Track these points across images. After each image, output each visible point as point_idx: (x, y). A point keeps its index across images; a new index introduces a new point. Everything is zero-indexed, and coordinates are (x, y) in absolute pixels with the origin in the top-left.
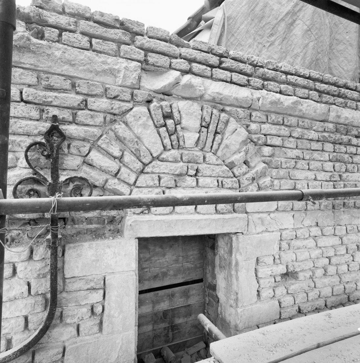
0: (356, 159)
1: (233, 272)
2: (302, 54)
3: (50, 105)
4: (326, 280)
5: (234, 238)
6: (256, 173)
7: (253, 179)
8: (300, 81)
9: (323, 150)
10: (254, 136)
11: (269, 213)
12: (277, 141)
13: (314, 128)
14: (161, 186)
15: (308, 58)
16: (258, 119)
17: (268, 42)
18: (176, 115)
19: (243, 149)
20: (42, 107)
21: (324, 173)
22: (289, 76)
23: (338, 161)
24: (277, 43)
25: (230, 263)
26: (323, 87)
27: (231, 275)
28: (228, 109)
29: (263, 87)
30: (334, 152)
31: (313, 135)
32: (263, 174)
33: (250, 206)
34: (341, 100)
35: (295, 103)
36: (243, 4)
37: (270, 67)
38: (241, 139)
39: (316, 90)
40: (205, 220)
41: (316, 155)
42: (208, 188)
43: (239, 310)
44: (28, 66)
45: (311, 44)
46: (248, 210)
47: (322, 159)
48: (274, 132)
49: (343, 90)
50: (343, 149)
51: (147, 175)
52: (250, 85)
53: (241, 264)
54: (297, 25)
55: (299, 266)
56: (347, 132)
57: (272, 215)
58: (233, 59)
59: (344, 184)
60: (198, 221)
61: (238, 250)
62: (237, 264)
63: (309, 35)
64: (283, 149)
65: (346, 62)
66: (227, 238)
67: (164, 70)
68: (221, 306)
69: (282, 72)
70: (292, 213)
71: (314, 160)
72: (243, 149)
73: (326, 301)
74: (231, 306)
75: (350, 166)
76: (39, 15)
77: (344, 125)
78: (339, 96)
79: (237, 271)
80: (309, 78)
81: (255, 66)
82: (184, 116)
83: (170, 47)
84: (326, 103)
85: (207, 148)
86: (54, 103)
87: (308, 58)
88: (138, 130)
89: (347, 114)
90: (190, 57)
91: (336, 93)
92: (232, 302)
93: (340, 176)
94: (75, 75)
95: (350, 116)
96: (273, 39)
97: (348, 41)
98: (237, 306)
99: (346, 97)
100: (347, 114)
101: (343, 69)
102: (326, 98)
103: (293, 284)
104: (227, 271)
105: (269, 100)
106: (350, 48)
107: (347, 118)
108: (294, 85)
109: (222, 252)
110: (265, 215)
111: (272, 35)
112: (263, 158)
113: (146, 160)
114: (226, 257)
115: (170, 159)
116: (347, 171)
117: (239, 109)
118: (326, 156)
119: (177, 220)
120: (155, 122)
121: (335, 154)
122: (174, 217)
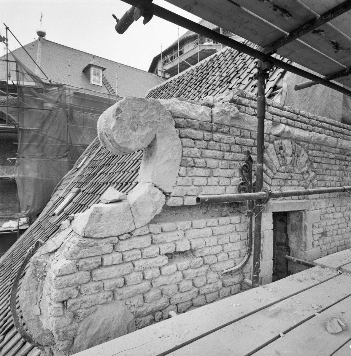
0: (350, 168)
1: (303, 232)
2: (320, 106)
3: (244, 145)
4: (338, 237)
5: (303, 213)
6: (312, 177)
7: (311, 181)
8: (326, 125)
9: (336, 164)
10: (311, 157)
11: (316, 199)
12: (319, 160)
13: (332, 152)
14: (220, 184)
15: (322, 109)
16: (312, 148)
17: (303, 99)
18: (284, 147)
19: (307, 165)
20: (241, 146)
21: (336, 177)
22: (322, 123)
23: (342, 170)
24: (307, 100)
25: (301, 227)
26: (335, 128)
27: (302, 233)
28: (301, 143)
29: (313, 130)
30: (340, 165)
31: (332, 156)
32: (314, 178)
33: (310, 196)
34: (342, 135)
35: (326, 138)
36: (294, 78)
37: (315, 119)
38: (306, 159)
39: (332, 130)
40: (296, 203)
41: (333, 167)
42: (201, 186)
43: (307, 252)
44: (237, 126)
45: (324, 100)
46: (309, 198)
47: (335, 169)
48: (318, 155)
49: (343, 130)
50: (343, 163)
51: (275, 180)
52: (308, 129)
53: (308, 227)
54: (318, 89)
55: (328, 228)
56: (344, 153)
57: (318, 200)
58: (302, 116)
59: (344, 183)
60: (294, 203)
61: (306, 219)
62: (305, 227)
63: (323, 95)
64: (321, 164)
65: (337, 109)
66: (298, 213)
67: (278, 123)
68: (293, 252)
69: (319, 121)
70: (325, 199)
71: (333, 170)
72: (307, 165)
73: (337, 249)
74: (302, 250)
75: (346, 173)
76: (240, 100)
77: (344, 149)
78: (341, 133)
79: (305, 231)
80: (330, 124)
81: (309, 118)
82: (286, 148)
83: (281, 112)
84: (336, 137)
85: (295, 165)
86: (246, 144)
87: (322, 109)
88: (272, 156)
89: (345, 143)
90: (287, 116)
91: (340, 131)
92: (302, 248)
93: (342, 178)
94: (251, 129)
95: (346, 144)
96: (305, 97)
97: (338, 97)
98: (305, 249)
99: (344, 134)
100: (345, 143)
101: (336, 113)
102: (337, 134)
103: (325, 239)
104: (298, 232)
105: (316, 137)
106: (339, 101)
107: (345, 146)
108: (324, 128)
109: (294, 221)
110: (315, 200)
111: (305, 95)
112: (312, 169)
113: (275, 172)
114: (297, 223)
115: (283, 171)
116: (345, 176)
117: (305, 143)
118: (337, 167)
119: (287, 203)
120: (277, 151)
121: (340, 166)
122: (285, 201)
